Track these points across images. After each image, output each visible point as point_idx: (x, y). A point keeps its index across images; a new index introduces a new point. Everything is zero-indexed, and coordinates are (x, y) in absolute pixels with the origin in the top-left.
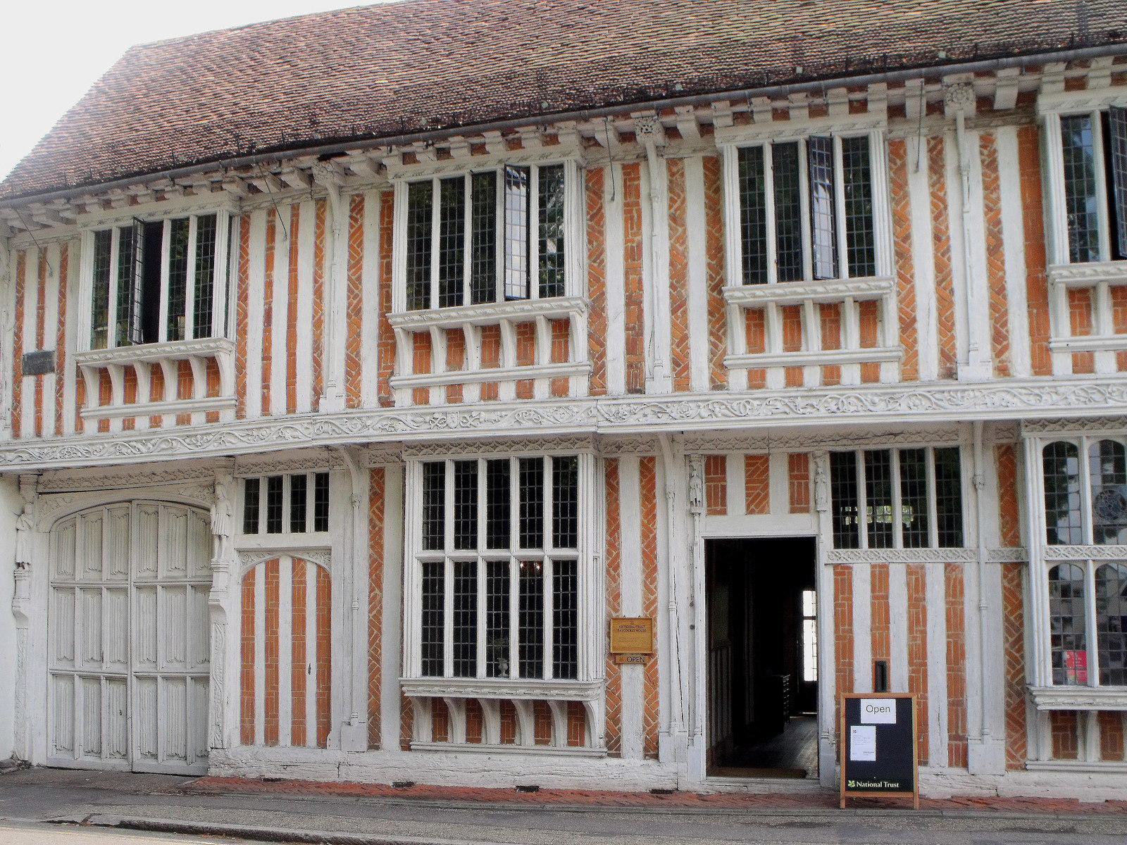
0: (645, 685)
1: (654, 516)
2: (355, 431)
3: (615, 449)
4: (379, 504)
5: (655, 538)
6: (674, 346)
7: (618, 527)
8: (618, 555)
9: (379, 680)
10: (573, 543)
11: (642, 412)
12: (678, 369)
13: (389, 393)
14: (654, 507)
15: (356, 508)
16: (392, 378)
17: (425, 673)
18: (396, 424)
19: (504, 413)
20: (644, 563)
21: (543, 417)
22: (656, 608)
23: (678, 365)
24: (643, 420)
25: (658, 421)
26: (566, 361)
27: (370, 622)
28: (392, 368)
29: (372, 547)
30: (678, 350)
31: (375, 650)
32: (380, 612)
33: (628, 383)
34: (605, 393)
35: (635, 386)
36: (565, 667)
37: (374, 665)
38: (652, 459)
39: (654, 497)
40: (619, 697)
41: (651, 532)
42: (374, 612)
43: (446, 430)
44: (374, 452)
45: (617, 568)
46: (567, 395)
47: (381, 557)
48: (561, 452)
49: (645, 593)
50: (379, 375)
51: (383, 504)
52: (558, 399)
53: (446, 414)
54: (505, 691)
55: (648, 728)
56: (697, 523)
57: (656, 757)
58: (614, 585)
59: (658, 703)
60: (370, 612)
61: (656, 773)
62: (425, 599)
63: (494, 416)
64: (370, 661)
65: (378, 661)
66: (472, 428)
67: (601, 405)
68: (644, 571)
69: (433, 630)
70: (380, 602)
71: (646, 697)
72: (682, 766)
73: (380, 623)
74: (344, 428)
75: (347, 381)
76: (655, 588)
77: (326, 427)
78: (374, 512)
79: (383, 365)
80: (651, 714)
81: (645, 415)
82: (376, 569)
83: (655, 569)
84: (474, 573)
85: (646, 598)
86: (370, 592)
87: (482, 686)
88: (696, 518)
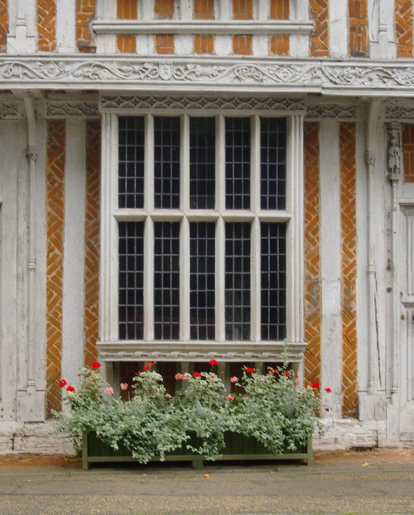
0: (344, 346)
1: (354, 182)
2: (52, 76)
3: (315, 113)
4: (58, 158)
5: (354, 203)
6: (398, 12)
7: (317, 191)
8: (317, 219)
9: (60, 346)
10: (282, 205)
11: (367, 76)
12: (401, 36)
13: (89, 37)
14: (353, 173)
15: (32, 163)
16: (95, 22)
17: (122, 336)
18: (99, 71)
19: (221, 68)
20: (343, 227)
21: (264, 74)
22: (355, 272)
23: (402, 32)
24: (368, 84)
25: (382, 86)
26: (287, 18)
27: (49, 283)
28: (93, 10)
29: (51, 204)
30: (402, 16)
31: (56, 315)
32: (60, 274)
33: (351, 45)
34: (327, 54)
35: (358, 46)
36: (273, 329)
37: (53, 330)
38: (352, 125)
39: (354, 162)
40: (319, 359)
41: (351, 196)
42: (54, 273)
43: (160, 81)
44: (54, 103)
45: (316, 231)
46: (287, 54)
47: (62, 215)
48: (270, 113)
49: (344, 256)
50: (78, 17)
51: (63, 158)
52: (277, 57)
53: (158, 64)
54: (176, 353)
55: (347, 388)
56: (395, 189)
57: (356, 415)
58: (312, 248)
59: (356, 363)
60: (49, 273)
61: (356, 431)
62: (122, 260)
63: (208, 70)
64: (48, 326)
65: (58, 325)
66: (187, 82)
67: (325, 67)
68: (343, 235)
69: (131, 292)
70: (61, 262)
71: (344, 358)
72: (381, 425)
73: (61, 284)
74: (37, 72)
75: (39, 21)
76: (355, 252)
77: (18, 71)
78: (52, 167)
79: (82, 6)
80: (349, 373)
81: (371, 80)
82: (55, 228)
83: (354, 233)
84: (248, 233)
85: (345, 261)
86: (49, 253)
87: (185, 346)
88: (395, 184)
